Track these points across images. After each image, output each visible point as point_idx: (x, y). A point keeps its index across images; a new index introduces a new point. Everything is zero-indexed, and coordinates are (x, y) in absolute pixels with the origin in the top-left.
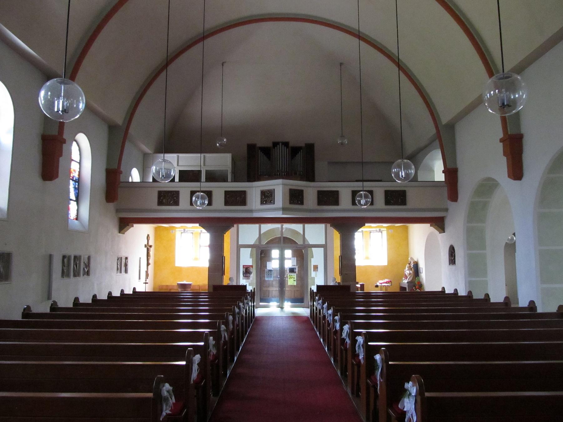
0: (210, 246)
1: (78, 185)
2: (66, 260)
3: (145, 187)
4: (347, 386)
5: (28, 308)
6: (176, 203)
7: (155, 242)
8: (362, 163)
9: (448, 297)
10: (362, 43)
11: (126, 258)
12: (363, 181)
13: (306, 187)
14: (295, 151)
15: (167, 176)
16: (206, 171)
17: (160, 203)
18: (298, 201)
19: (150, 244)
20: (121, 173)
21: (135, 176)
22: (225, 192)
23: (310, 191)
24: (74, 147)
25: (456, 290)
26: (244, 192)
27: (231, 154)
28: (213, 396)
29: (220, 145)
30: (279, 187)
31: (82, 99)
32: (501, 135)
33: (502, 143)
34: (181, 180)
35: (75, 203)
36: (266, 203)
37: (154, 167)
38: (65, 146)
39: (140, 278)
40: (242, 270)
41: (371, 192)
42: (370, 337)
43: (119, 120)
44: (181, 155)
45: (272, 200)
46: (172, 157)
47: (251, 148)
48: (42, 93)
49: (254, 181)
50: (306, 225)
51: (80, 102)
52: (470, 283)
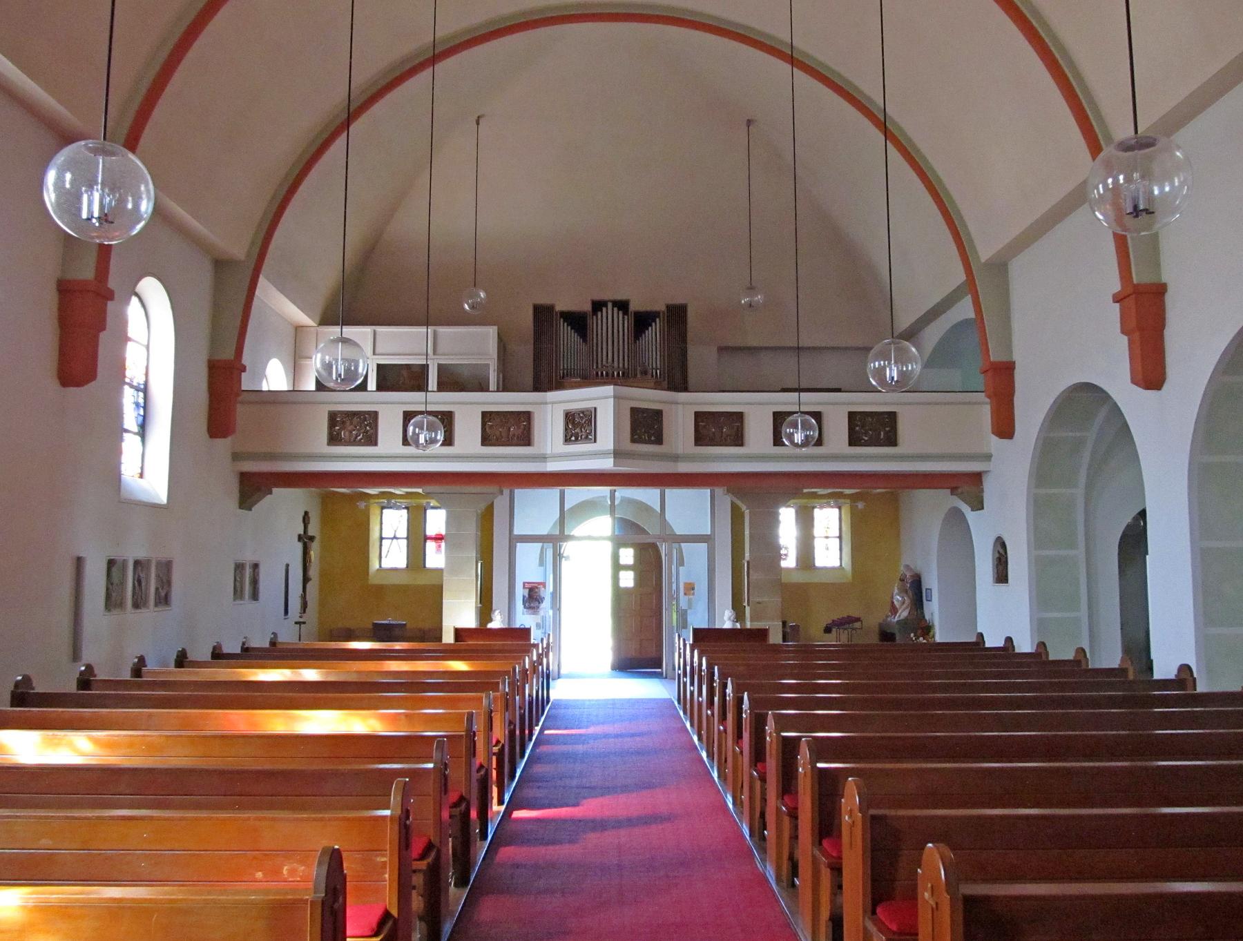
1: (145, 398)
2: (114, 569)
4: (763, 860)
5: (27, 680)
8: (799, 349)
9: (1021, 665)
10: (801, 76)
11: (256, 566)
14: (642, 321)
15: (350, 374)
16: (440, 366)
19: (310, 533)
20: (243, 369)
21: (275, 377)
22: (484, 414)
23: (680, 411)
24: (133, 309)
25: (1009, 640)
26: (528, 416)
27: (496, 328)
28: (455, 885)
29: (472, 307)
31: (148, 191)
32: (1116, 287)
33: (1117, 305)
34: (380, 388)
35: (138, 438)
36: (577, 439)
37: (319, 355)
38: (111, 306)
39: (286, 612)
40: (520, 592)
41: (817, 416)
42: (822, 750)
43: (238, 249)
44: (380, 329)
46: (361, 334)
47: (542, 313)
48: (51, 176)
50: (668, 491)
51: (140, 198)
52: (1039, 625)
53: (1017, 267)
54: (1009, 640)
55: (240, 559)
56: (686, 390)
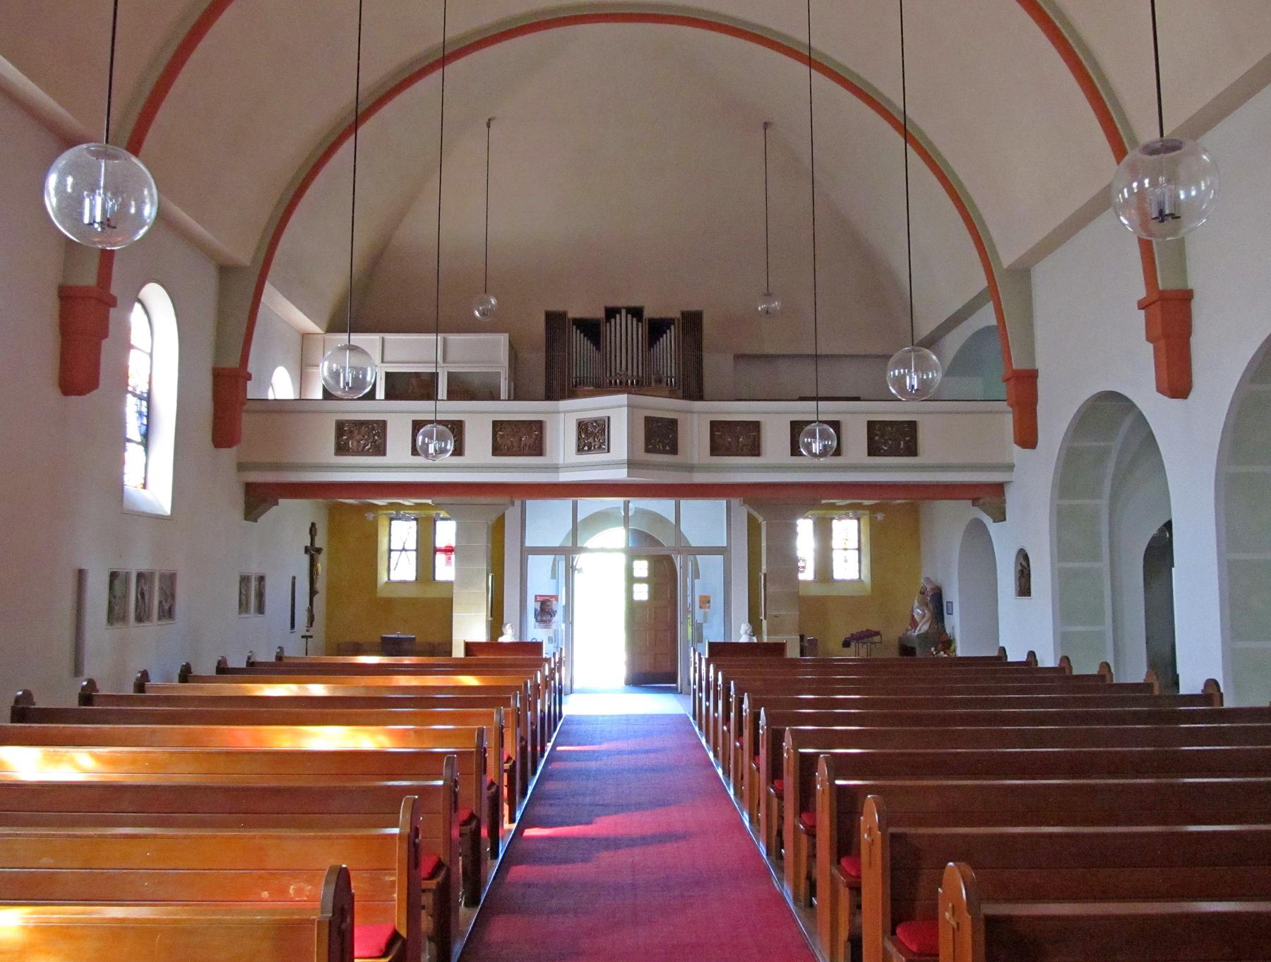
0: (130, 347)
1: (149, 407)
2: (117, 582)
4: (781, 880)
5: (27, 695)
8: (817, 357)
10: (819, 78)
11: (261, 579)
14: (657, 329)
15: (358, 383)
16: (450, 374)
19: (317, 545)
20: (249, 377)
21: (281, 386)
22: (495, 423)
23: (696, 420)
24: (136, 316)
25: (1032, 654)
26: (539, 425)
27: (507, 335)
28: (466, 905)
29: (483, 314)
31: (151, 195)
32: (1141, 293)
33: (1143, 312)
34: (389, 396)
35: (141, 448)
36: (590, 449)
37: (326, 363)
38: (113, 312)
39: (293, 626)
40: (532, 606)
41: (836, 425)
43: (244, 254)
44: (388, 336)
46: (369, 341)
47: (555, 320)
48: (52, 180)
50: (683, 502)
51: (144, 202)
52: (1063, 639)
53: (1040, 273)
54: (1032, 654)
55: (246, 572)
56: (701, 398)
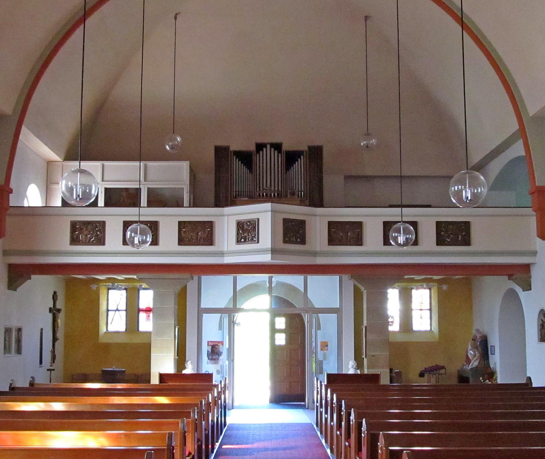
3: (58, 215)
6: (101, 241)
7: (66, 303)
11: (19, 330)
12: (402, 206)
13: (217, 216)
14: (291, 158)
15: (86, 195)
16: (149, 189)
17: (74, 241)
18: (296, 239)
19: (58, 306)
21: (33, 197)
23: (318, 220)
29: (172, 148)
30: (263, 213)
34: (107, 204)
36: (245, 241)
39: (41, 362)
40: (205, 348)
41: (414, 224)
44: (106, 163)
45: (254, 237)
46: (93, 166)
47: (221, 152)
49: (226, 205)
